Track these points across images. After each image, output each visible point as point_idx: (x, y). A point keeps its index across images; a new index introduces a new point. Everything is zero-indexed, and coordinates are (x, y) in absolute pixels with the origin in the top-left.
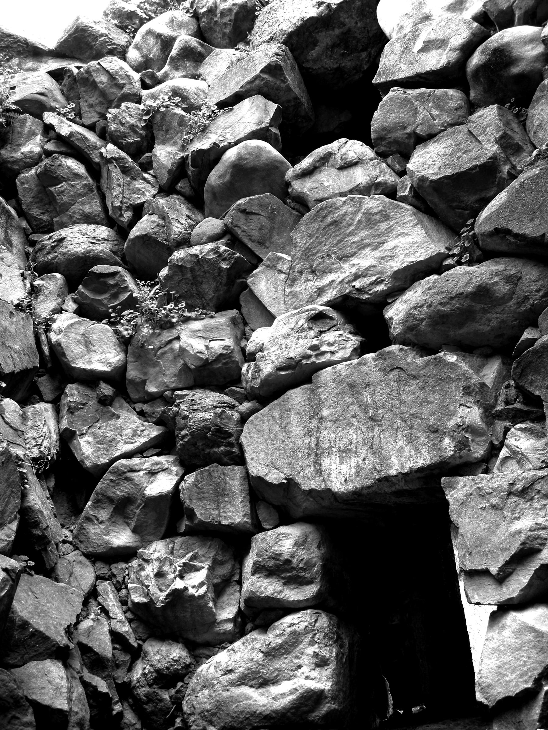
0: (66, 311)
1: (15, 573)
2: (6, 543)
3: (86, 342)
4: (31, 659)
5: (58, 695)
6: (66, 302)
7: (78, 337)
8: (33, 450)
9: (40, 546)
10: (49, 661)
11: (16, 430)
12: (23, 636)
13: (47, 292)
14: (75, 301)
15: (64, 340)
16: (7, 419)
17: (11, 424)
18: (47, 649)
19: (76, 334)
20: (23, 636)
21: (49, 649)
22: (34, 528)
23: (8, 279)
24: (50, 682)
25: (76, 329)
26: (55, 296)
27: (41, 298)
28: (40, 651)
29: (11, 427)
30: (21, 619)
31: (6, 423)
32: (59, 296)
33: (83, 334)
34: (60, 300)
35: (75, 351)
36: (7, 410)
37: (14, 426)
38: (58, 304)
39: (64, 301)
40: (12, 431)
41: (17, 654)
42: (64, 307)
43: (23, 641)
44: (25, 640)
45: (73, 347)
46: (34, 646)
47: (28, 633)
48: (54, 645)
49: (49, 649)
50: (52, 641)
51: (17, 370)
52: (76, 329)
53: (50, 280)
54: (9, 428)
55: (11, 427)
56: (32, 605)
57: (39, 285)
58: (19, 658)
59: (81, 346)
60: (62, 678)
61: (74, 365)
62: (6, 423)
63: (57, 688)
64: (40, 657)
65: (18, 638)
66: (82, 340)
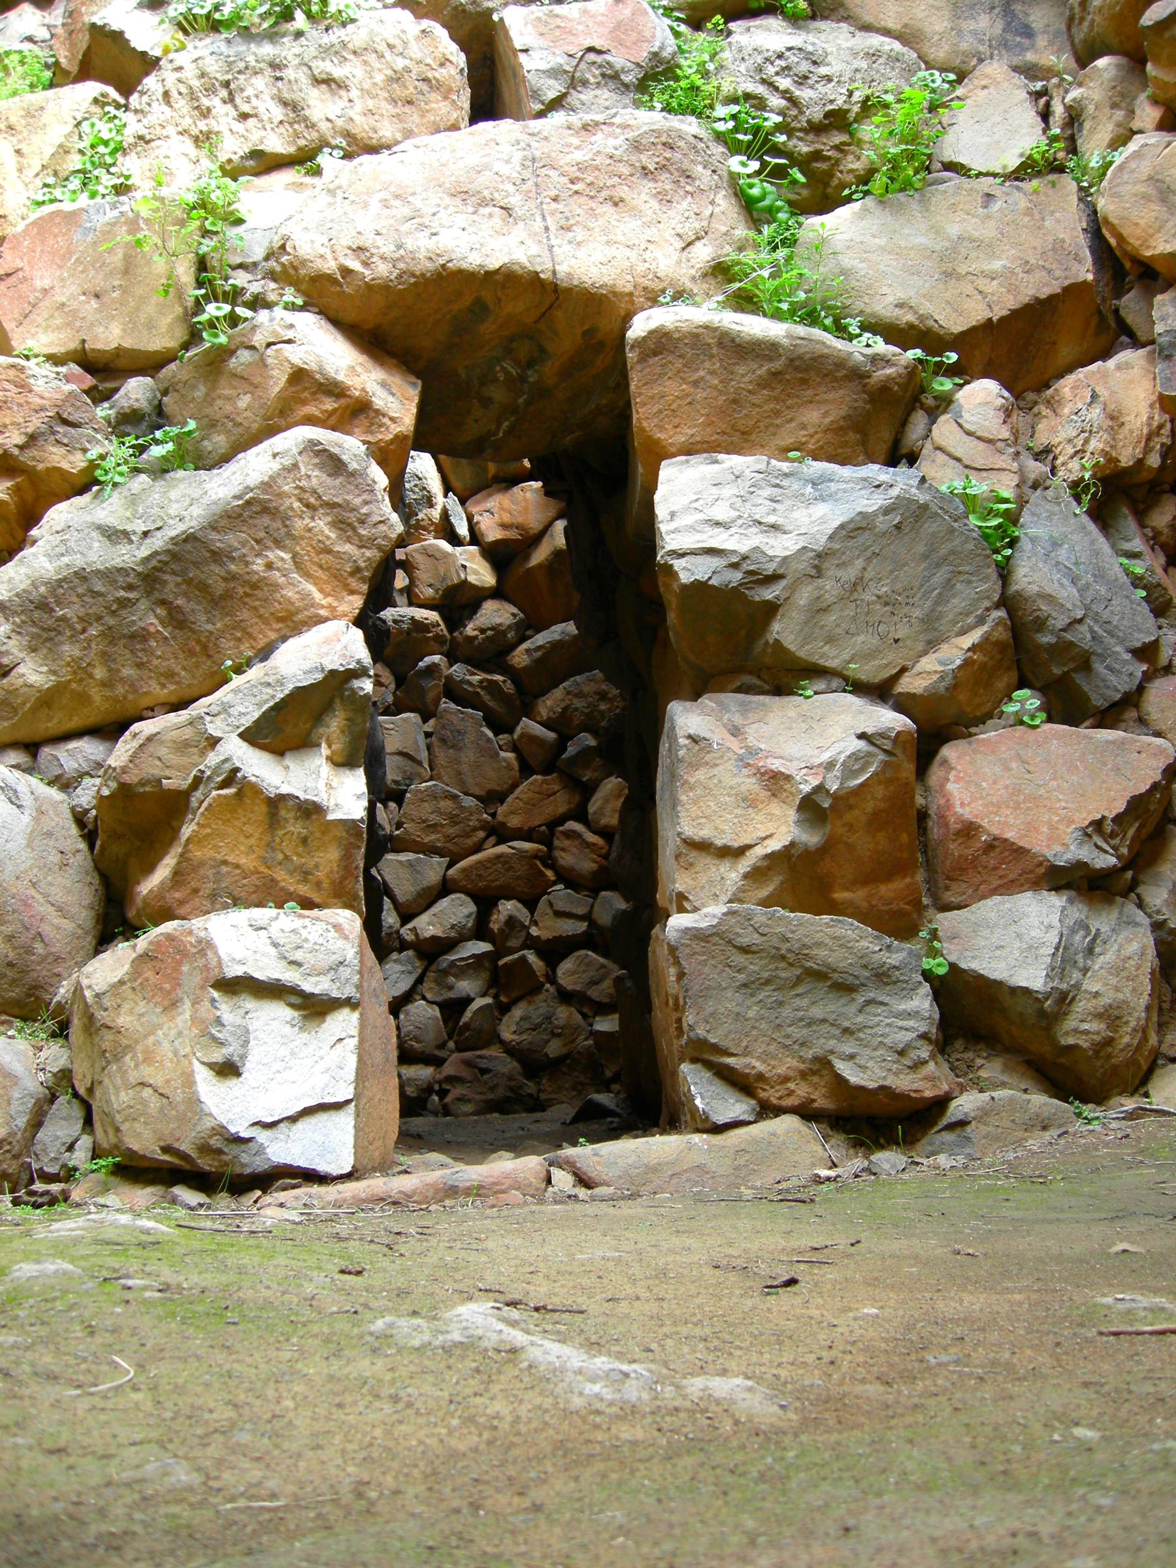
0: (1140, 132)
1: (889, 738)
2: (935, 677)
3: (1161, 192)
4: (994, 892)
5: (1029, 960)
6: (1138, 112)
7: (1141, 188)
8: (1070, 466)
9: (1065, 665)
10: (1029, 894)
11: (990, 441)
12: (970, 851)
13: (1091, 108)
14: (1155, 101)
15: (1112, 207)
16: (967, 426)
17: (979, 434)
18: (1024, 872)
19: (1135, 184)
20: (970, 851)
21: (1031, 872)
22: (1038, 631)
23: (999, 119)
24: (1019, 936)
25: (1132, 172)
26: (1107, 110)
27: (1087, 125)
28: (1011, 876)
29: (979, 438)
30: (960, 819)
31: (969, 434)
32: (1114, 106)
33: (1150, 178)
34: (1119, 115)
35: (1142, 222)
36: (966, 406)
37: (986, 435)
38: (1119, 125)
39: (1133, 112)
40: (982, 446)
41: (964, 885)
42: (1136, 125)
43: (972, 862)
44: (975, 858)
45: (1134, 215)
46: (994, 869)
47: (978, 845)
48: (1040, 864)
49: (1031, 872)
50: (1035, 855)
51: (998, 313)
52: (1132, 172)
53: (1092, 80)
54: (976, 442)
55: (979, 438)
56: (1006, 787)
57: (1074, 100)
58: (970, 891)
59: (1153, 206)
60: (1050, 927)
61: (1148, 253)
62: (969, 434)
63: (1030, 947)
64: (1009, 887)
65: (961, 856)
66: (1151, 191)
